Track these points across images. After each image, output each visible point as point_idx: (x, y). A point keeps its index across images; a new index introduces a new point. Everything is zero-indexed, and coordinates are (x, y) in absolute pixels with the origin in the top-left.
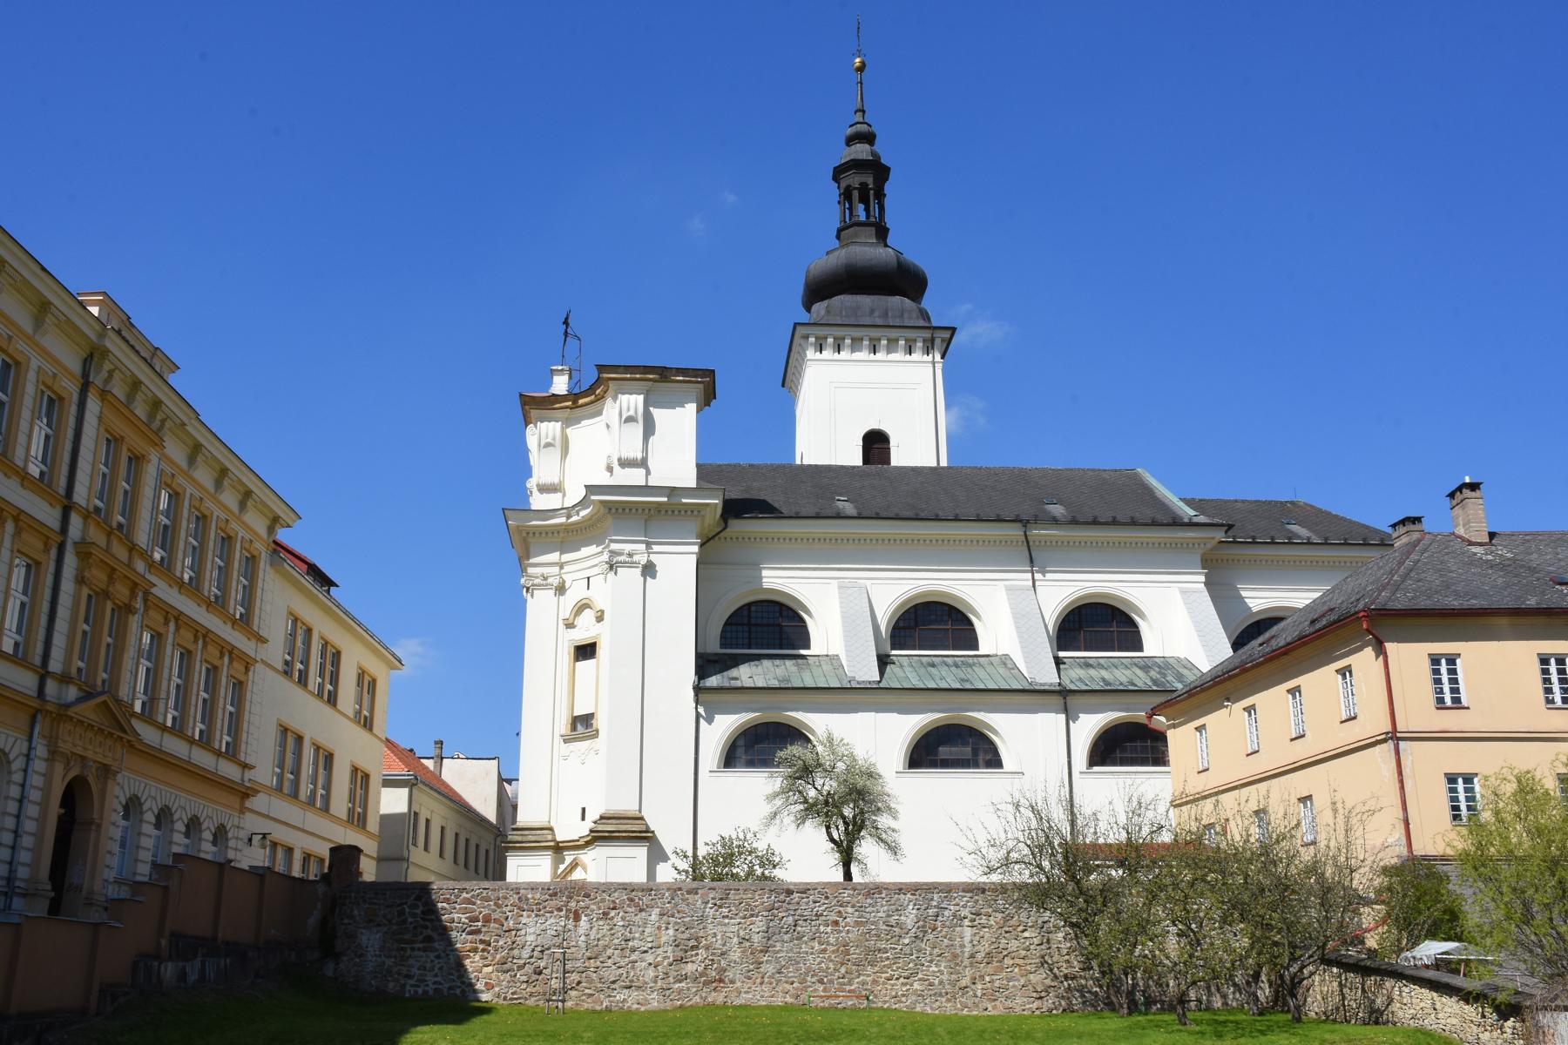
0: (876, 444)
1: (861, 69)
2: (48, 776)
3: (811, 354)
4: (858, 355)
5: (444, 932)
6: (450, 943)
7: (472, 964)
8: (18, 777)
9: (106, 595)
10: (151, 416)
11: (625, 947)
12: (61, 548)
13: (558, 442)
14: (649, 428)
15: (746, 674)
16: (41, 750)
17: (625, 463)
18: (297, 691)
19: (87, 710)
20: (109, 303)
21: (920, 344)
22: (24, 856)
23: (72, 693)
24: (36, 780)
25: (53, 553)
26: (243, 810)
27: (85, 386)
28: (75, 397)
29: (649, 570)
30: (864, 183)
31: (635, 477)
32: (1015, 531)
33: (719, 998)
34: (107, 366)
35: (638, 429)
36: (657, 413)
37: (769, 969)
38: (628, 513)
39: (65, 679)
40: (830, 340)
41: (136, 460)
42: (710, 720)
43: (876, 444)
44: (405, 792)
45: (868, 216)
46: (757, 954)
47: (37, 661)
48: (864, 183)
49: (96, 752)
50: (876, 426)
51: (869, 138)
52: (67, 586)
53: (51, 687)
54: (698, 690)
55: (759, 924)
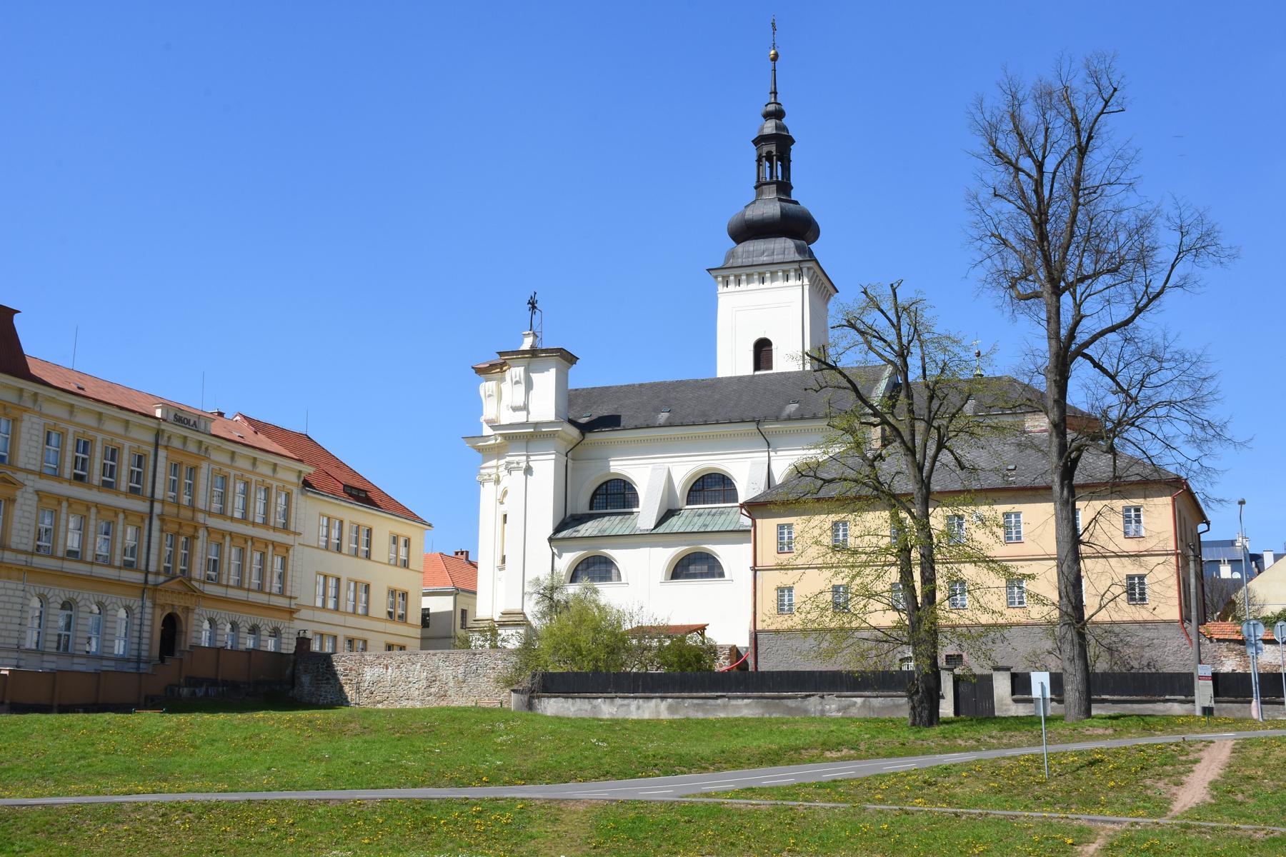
0: (762, 350)
1: (775, 58)
2: (153, 614)
3: (721, 289)
4: (752, 286)
5: (335, 674)
6: (338, 680)
7: (346, 688)
8: (138, 616)
9: (178, 534)
10: (200, 448)
11: (407, 681)
12: (151, 519)
13: (495, 394)
14: (529, 386)
15: (587, 529)
16: (148, 604)
17: (515, 409)
18: (337, 556)
19: (173, 585)
20: (166, 406)
21: (792, 274)
22: (144, 647)
23: (162, 579)
24: (148, 616)
25: (147, 522)
26: (292, 619)
27: (157, 446)
28: (152, 452)
29: (528, 471)
30: (777, 148)
31: (520, 417)
32: (752, 427)
33: (444, 704)
34: (166, 435)
35: (522, 388)
36: (534, 376)
37: (465, 690)
38: (526, 438)
39: (157, 573)
40: (732, 278)
41: (193, 471)
42: (560, 557)
43: (762, 350)
44: (451, 598)
45: (771, 177)
46: (461, 683)
47: (143, 568)
48: (777, 148)
49: (179, 602)
50: (762, 336)
51: (778, 114)
52: (155, 534)
53: (151, 578)
54: (550, 540)
55: (461, 669)
